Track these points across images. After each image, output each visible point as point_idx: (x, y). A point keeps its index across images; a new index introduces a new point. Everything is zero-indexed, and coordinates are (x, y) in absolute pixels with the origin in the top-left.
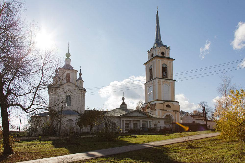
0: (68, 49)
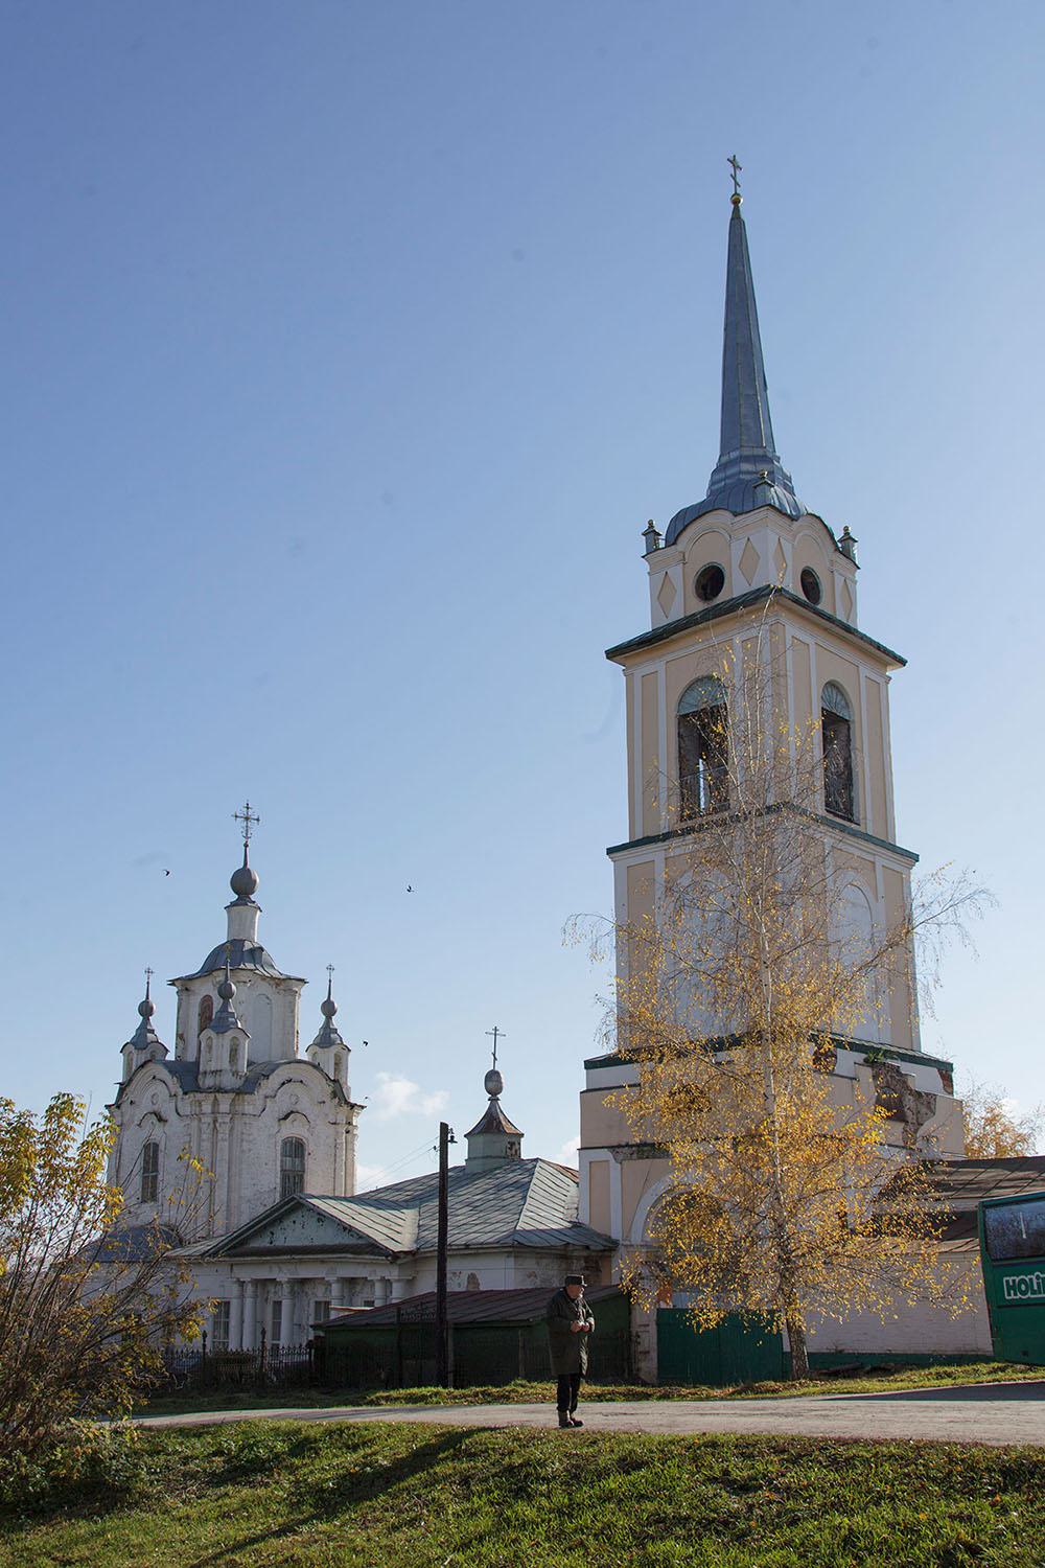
0: (246, 846)
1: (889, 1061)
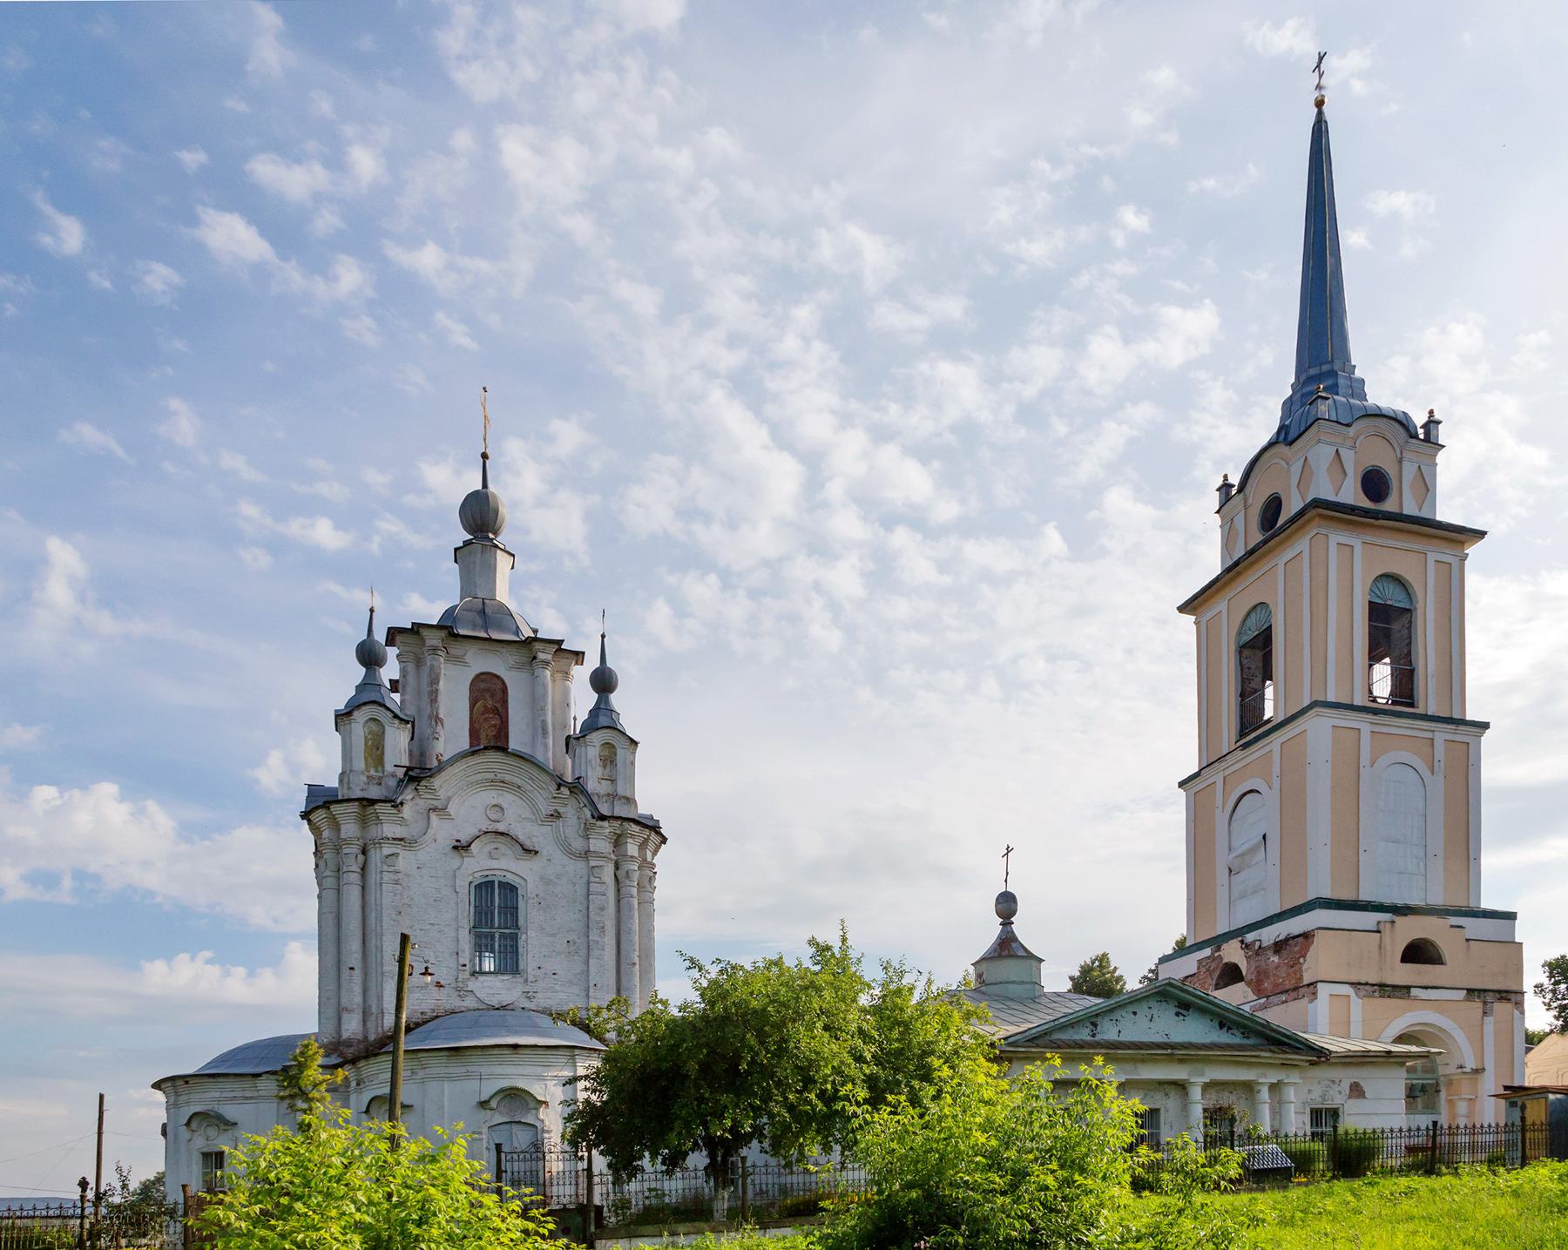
1: (483, 916)
